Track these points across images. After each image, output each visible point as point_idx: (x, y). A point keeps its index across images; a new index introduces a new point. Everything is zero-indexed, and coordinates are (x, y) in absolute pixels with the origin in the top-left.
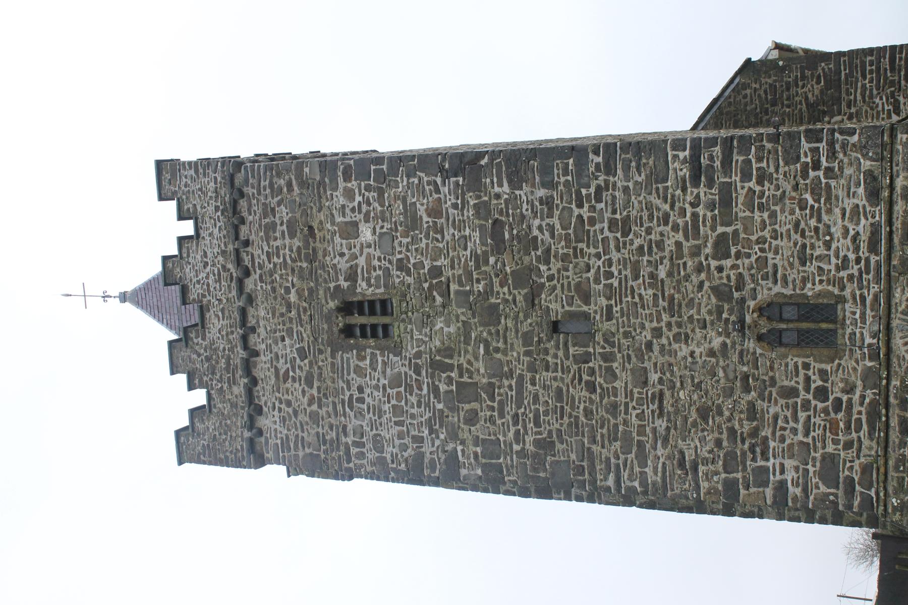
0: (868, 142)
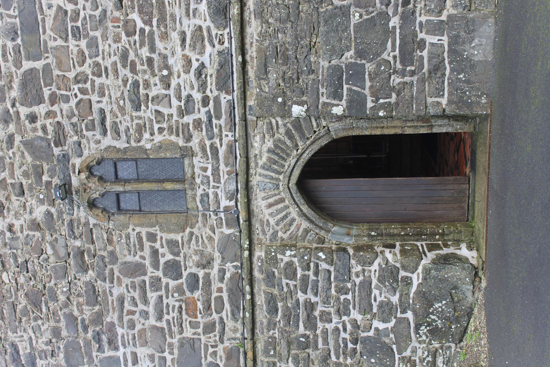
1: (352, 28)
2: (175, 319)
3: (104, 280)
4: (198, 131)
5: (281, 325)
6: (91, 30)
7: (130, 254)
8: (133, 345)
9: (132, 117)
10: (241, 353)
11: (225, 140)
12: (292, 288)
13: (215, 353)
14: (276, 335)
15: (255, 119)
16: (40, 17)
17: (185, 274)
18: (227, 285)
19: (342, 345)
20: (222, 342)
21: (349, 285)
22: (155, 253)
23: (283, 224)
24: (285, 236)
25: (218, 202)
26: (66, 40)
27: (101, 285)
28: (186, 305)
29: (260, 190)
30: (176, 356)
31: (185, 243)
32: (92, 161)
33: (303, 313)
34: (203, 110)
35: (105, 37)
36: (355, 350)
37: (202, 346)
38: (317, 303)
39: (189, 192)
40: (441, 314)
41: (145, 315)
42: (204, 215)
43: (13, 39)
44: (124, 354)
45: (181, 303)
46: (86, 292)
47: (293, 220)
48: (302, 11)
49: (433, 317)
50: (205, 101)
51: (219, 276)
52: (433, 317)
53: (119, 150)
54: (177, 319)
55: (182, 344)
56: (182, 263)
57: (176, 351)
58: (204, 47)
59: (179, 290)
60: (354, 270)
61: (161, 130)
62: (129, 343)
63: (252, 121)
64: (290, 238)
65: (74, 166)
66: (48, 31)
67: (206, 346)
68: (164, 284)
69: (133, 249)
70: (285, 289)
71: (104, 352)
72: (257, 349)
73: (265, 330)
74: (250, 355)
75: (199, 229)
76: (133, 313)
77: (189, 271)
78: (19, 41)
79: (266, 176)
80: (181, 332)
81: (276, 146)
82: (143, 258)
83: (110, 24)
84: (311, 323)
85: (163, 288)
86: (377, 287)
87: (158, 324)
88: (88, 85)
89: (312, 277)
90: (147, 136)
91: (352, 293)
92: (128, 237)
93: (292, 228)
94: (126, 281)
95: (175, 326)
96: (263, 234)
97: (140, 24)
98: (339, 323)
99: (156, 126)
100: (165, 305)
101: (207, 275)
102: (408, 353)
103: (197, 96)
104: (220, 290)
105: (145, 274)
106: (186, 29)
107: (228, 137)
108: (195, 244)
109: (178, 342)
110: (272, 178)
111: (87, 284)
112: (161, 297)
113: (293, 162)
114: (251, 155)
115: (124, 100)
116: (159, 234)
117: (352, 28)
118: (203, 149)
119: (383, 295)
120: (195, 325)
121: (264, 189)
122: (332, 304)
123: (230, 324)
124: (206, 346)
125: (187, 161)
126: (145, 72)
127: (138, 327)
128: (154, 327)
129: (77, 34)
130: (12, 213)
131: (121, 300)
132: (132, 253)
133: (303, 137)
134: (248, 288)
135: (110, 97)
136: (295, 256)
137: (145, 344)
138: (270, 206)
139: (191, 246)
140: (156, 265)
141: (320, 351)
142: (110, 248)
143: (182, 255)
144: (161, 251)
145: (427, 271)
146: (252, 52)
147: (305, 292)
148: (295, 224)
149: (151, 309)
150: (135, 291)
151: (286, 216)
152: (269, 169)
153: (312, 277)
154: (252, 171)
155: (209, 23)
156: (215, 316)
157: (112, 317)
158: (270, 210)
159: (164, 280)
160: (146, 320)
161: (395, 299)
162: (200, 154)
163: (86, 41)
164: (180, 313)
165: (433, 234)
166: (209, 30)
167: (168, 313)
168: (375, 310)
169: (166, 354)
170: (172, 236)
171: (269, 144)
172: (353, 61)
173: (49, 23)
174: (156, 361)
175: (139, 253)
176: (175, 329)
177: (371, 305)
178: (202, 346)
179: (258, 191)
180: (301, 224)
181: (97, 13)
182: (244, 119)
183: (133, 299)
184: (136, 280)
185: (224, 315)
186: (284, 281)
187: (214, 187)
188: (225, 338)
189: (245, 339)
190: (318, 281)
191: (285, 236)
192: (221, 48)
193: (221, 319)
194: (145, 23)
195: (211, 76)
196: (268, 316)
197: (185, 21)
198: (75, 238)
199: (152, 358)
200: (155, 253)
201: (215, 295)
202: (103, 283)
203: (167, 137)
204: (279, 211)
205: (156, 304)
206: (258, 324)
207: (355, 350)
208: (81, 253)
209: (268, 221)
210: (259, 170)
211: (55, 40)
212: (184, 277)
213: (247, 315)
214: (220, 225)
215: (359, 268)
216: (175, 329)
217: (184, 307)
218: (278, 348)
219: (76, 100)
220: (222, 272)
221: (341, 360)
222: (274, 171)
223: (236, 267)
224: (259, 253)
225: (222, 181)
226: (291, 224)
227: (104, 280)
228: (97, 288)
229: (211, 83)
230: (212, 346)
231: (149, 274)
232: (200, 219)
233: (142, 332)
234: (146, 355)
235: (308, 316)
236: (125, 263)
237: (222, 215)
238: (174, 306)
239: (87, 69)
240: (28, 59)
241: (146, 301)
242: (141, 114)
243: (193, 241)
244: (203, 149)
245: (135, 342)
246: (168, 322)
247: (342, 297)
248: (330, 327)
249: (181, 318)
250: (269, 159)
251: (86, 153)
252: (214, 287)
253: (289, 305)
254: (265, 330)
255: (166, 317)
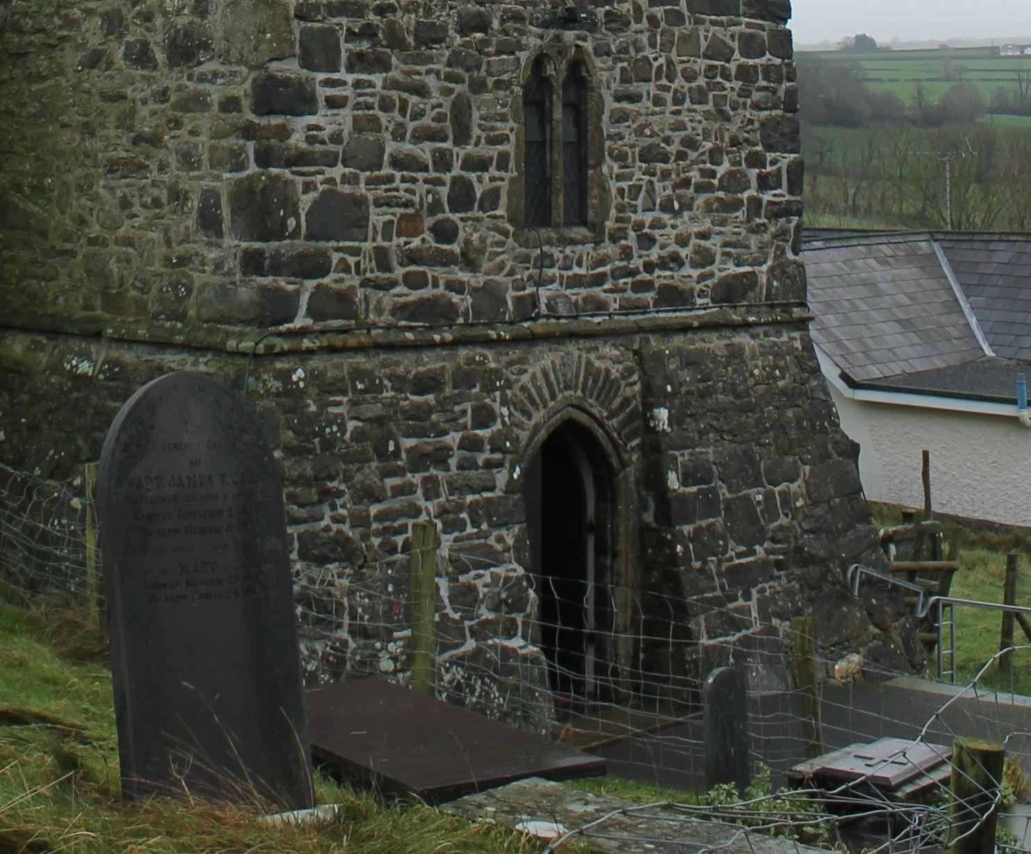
0: (788, 278)
2: (396, 193)
3: (449, 64)
4: (621, 254)
5: (402, 403)
6: (714, 96)
7: (482, 118)
8: (358, 103)
9: (632, 146)
10: (347, 322)
12: (461, 421)
13: (347, 269)
14: (385, 394)
15: (636, 347)
16: (724, 18)
17: (456, 217)
18: (442, 295)
19: (396, 524)
20: (364, 284)
21: (484, 526)
23: (523, 398)
26: (706, 56)
27: (442, 55)
28: (412, 215)
29: (562, 358)
31: (494, 221)
32: (588, 71)
33: (428, 444)
36: (393, 550)
37: (356, 244)
38: (448, 469)
44: (344, 83)
45: (418, 206)
46: (433, 24)
47: (530, 417)
48: (747, 417)
51: (454, 281)
54: (395, 197)
55: (359, 202)
56: (469, 214)
60: (504, 532)
62: (360, 95)
63: (632, 342)
65: (584, 39)
68: (442, 176)
69: (489, 124)
70: (457, 408)
71: (346, 41)
72: (353, 354)
73: (388, 371)
75: (513, 249)
76: (403, 111)
79: (579, 367)
80: (377, 203)
83: (717, 126)
84: (419, 460)
85: (438, 175)
86: (495, 577)
88: (664, 82)
89: (481, 458)
91: (475, 534)
92: (503, 118)
95: (386, 191)
96: (507, 363)
98: (428, 514)
100: (414, 174)
105: (456, 143)
106: (712, 241)
108: (496, 239)
109: (361, 195)
111: (444, 28)
113: (595, 411)
114: (599, 342)
115: (651, 136)
116: (507, 175)
119: (486, 590)
121: (564, 364)
122: (451, 498)
127: (383, 117)
131: (421, 91)
132: (483, 122)
133: (623, 424)
135: (654, 114)
136: (503, 423)
137: (358, 126)
139: (492, 233)
141: (379, 483)
142: (490, 81)
143: (480, 214)
144: (486, 176)
147: (462, 446)
148: (524, 419)
149: (407, 147)
150: (434, 120)
151: (533, 402)
153: (481, 458)
155: (719, 275)
156: (399, 272)
158: (539, 375)
160: (392, 134)
163: (704, 85)
167: (403, 180)
168: (462, 579)
172: (721, 498)
174: (333, 146)
175: (484, 135)
176: (381, 191)
178: (356, 244)
179: (562, 354)
180: (524, 430)
184: (448, 123)
186: (468, 406)
187: (562, 277)
188: (369, 291)
189: (369, 330)
190: (477, 470)
193: (393, 284)
195: (672, 277)
196: (411, 377)
198: (503, 21)
202: (445, 59)
203: (614, 203)
205: (415, 158)
207: (393, 550)
208: (484, 26)
209: (526, 371)
211: (706, 38)
212: (451, 215)
215: (510, 541)
216: (381, 191)
217: (411, 211)
218: (368, 396)
219: (651, 57)
221: (375, 526)
222: (586, 380)
225: (568, 292)
228: (437, 46)
230: (358, 264)
231: (455, 150)
232: (523, 250)
233: (375, 124)
234: (341, 127)
235: (428, 455)
236: (470, 107)
238: (413, 192)
243: (499, 237)
245: (361, 109)
246: (390, 179)
247: (464, 515)
248: (419, 498)
249: (398, 205)
251: (598, 63)
252: (439, 272)
253: (434, 417)
254: (388, 371)
255: (398, 175)
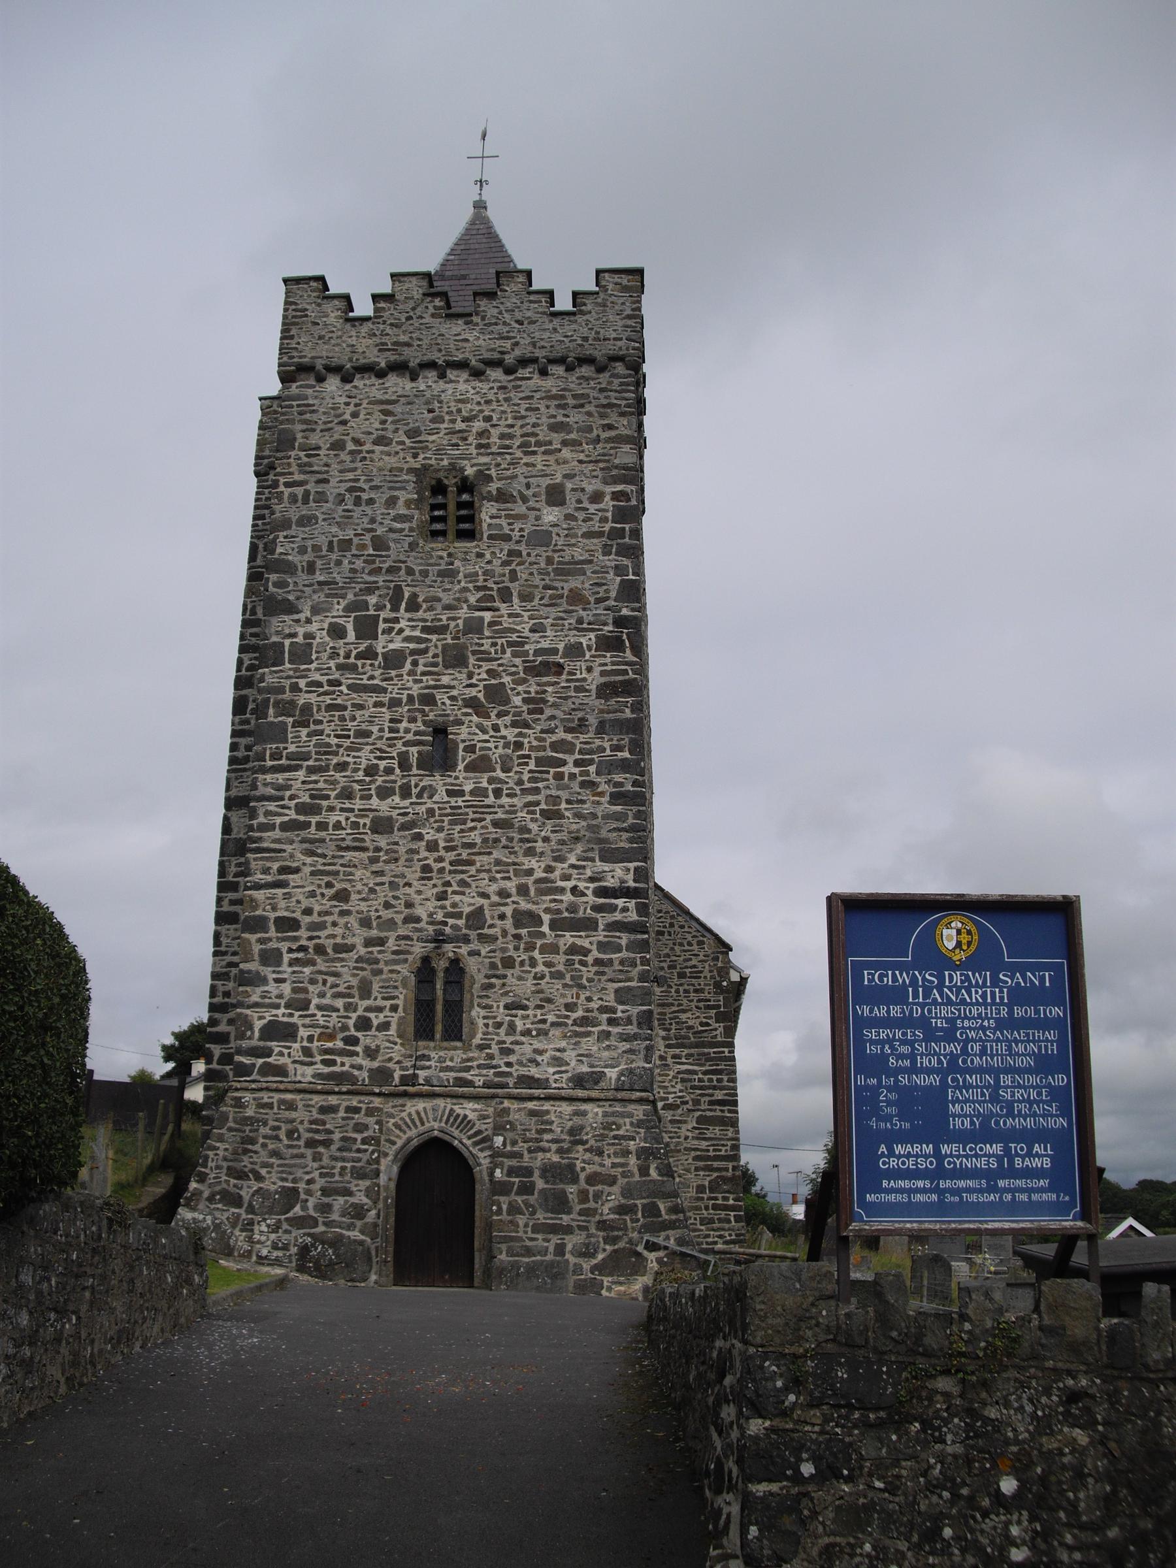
1: (561, 1186)
11: (476, 1079)
22: (380, 1009)
24: (390, 1125)
25: (423, 1068)
30: (281, 1019)
34: (501, 1063)
35: (565, 986)
39: (432, 1044)
40: (322, 1255)
41: (322, 995)
42: (411, 1056)
43: (567, 910)
47: (405, 1133)
49: (320, 1248)
50: (509, 1064)
52: (320, 1248)
53: (471, 987)
57: (285, 1019)
58: (554, 1066)
59: (345, 1028)
61: (487, 1025)
64: (388, 1129)
65: (460, 947)
66: (572, 940)
67: (290, 1048)
74: (282, 1087)
77: (362, 1038)
78: (566, 914)
80: (304, 1026)
81: (469, 1122)
82: (376, 999)
87: (312, 1006)
89: (355, 1147)
90: (483, 1013)
92: (396, 987)
93: (397, 1132)
94: (354, 982)
97: (574, 1015)
99: (490, 1022)
101: (357, 1054)
102: (285, 1226)
103: (512, 1059)
104: (343, 1064)
107: (479, 1081)
110: (442, 1116)
112: (338, 1010)
114: (462, 1101)
116: (396, 1016)
117: (561, 1186)
118: (469, 1060)
120: (310, 1039)
123: (309, 1071)
124: (290, 1048)
125: (459, 1044)
126: (535, 1016)
128: (310, 1002)
129: (570, 963)
130: (422, 888)
134: (344, 1089)
137: (295, 990)
138: (418, 1113)
140: (368, 1009)
144: (381, 1016)
145: (361, 1243)
146: (547, 1106)
148: (401, 1134)
149: (326, 1001)
151: (409, 1127)
152: (450, 1115)
154: (448, 1100)
156: (318, 1058)
157: (321, 965)
158: (413, 1113)
159: (354, 1016)
161: (335, 1216)
162: (464, 1056)
164: (323, 1027)
165: (386, 1253)
166: (566, 1072)
169: (282, 1010)
170: (394, 1027)
171: (472, 1116)
173: (579, 942)
177: (329, 1196)
181: (584, 981)
182: (493, 1097)
183: (337, 986)
185: (319, 1066)
191: (390, 1125)
192: (551, 1081)
193: (316, 1063)
194: (575, 1020)
197: (574, 1053)
199: (280, 996)
200: (380, 1009)
201: (339, 1060)
204: (413, 1121)
206: (308, 1096)
210: (449, 1107)
213: (319, 1087)
214: (403, 1069)
216: (307, 1021)
220: (360, 1068)
223: (364, 1080)
224: (377, 1102)
226: (401, 1130)
227: (357, 962)
229: (524, 1071)
230: (289, 1054)
233: (306, 991)
237: (411, 1072)
239: (541, 968)
240: (551, 920)
241: (337, 995)
242: (501, 1010)
243: (388, 1044)
244: (469, 1060)
246: (314, 1015)
250: (458, 1115)
252: (346, 1060)
255: (319, 1014)
